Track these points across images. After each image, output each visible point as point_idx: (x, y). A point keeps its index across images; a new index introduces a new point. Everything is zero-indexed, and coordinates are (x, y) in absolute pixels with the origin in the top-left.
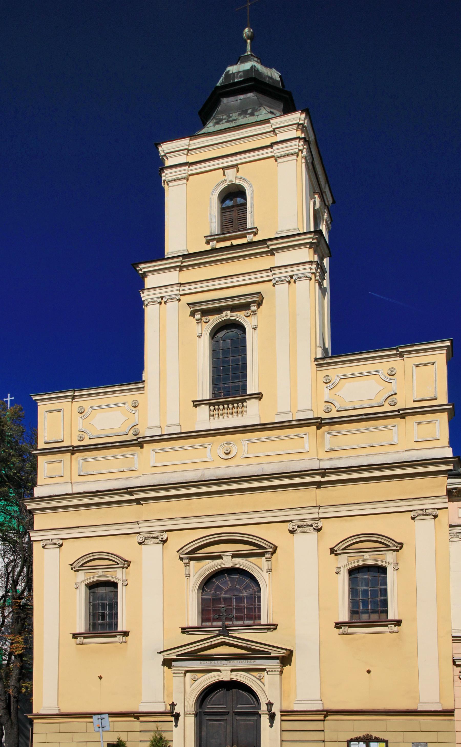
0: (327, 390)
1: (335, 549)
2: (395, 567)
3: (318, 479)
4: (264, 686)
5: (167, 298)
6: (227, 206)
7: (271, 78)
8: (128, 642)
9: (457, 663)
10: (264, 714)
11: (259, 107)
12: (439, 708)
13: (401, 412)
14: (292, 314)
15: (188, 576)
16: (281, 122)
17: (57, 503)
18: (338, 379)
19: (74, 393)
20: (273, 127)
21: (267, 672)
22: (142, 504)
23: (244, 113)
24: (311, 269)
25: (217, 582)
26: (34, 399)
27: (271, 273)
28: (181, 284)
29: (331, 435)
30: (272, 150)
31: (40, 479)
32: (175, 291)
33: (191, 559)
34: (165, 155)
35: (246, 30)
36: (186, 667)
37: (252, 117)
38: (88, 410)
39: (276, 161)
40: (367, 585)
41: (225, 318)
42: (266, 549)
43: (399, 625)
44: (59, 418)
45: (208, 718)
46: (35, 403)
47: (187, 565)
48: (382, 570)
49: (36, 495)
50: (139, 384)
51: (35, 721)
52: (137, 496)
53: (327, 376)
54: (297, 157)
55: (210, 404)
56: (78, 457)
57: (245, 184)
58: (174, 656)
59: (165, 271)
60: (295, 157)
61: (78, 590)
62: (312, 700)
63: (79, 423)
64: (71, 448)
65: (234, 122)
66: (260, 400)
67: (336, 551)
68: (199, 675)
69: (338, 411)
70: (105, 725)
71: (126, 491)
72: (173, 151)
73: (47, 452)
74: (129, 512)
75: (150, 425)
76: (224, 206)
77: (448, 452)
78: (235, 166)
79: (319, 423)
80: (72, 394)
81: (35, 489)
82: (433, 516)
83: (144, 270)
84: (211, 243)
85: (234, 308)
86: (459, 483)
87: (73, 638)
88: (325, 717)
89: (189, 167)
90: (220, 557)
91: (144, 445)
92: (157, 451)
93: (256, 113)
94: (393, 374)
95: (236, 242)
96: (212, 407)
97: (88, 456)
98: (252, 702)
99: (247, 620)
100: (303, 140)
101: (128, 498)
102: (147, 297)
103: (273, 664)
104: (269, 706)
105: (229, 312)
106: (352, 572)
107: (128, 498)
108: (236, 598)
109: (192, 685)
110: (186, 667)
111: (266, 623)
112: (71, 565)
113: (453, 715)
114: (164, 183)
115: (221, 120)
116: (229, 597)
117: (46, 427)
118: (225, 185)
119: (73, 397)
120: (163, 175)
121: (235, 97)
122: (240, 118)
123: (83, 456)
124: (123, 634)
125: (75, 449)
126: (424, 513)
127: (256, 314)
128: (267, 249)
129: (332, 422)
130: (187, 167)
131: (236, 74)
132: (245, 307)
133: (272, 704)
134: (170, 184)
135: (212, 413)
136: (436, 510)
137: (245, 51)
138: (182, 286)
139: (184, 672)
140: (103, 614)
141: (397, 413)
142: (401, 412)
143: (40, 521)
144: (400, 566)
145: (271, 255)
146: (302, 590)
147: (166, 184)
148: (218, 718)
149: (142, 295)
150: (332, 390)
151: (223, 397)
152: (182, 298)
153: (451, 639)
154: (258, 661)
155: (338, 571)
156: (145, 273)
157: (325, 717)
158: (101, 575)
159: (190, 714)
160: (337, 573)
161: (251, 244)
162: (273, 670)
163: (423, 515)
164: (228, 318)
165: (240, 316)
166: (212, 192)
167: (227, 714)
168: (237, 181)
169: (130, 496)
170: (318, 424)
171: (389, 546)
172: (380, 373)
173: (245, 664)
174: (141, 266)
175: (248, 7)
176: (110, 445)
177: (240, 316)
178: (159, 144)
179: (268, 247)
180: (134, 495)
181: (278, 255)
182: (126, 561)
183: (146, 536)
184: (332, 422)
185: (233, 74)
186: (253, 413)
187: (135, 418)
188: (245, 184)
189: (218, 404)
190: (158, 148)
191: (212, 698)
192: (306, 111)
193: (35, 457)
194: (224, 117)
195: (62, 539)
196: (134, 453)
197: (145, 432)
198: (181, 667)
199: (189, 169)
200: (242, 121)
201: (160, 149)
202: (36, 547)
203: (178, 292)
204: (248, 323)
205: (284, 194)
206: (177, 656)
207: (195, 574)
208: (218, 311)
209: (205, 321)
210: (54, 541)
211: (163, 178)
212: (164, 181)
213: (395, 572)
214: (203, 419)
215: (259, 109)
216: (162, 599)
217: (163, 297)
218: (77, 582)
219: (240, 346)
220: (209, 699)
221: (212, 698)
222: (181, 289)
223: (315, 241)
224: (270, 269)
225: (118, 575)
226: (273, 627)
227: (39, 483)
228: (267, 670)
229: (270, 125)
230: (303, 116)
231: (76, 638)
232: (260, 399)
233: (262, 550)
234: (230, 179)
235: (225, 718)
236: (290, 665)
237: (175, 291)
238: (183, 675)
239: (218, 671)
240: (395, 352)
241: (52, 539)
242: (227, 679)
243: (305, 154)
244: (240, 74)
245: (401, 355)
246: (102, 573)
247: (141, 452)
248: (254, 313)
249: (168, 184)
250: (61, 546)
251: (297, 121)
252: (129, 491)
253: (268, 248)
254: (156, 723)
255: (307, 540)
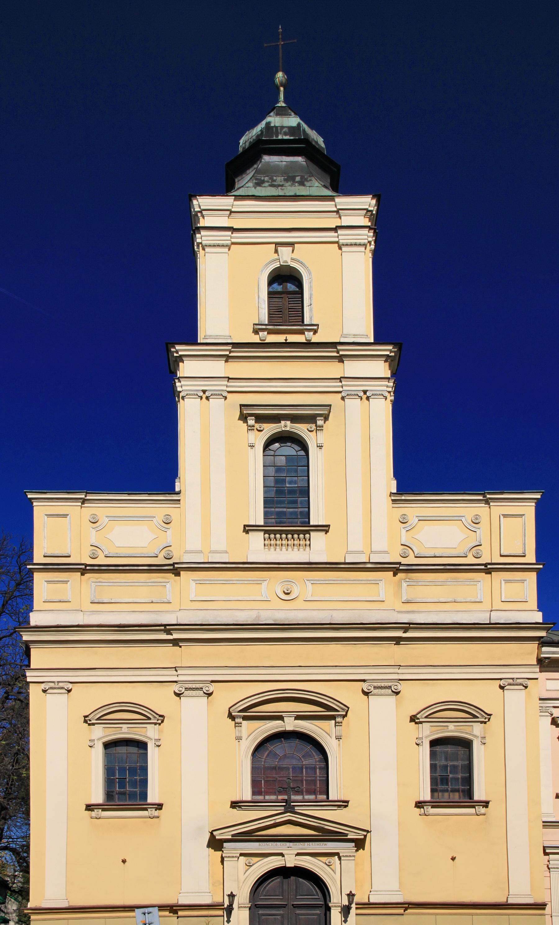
0: (404, 531)
1: (418, 716)
2: (158, 743)
3: (399, 634)
4: (335, 873)
5: (211, 393)
6: (274, 290)
7: (317, 142)
8: (161, 817)
9: (547, 851)
10: (335, 906)
11: (310, 176)
12: (531, 901)
13: (489, 566)
14: (357, 443)
15: (239, 739)
16: (347, 203)
17: (65, 635)
18: (417, 520)
19: (86, 496)
20: (338, 207)
21: (340, 859)
22: (180, 647)
23: (291, 179)
24: (387, 386)
25: (270, 747)
26: (29, 496)
27: (340, 384)
28: (229, 378)
29: (408, 583)
30: (336, 234)
31: (37, 603)
32: (222, 386)
33: (245, 718)
34: (201, 212)
35: (280, 75)
36: (241, 849)
37: (302, 188)
38: (103, 520)
39: (340, 248)
40: (446, 759)
41: (283, 429)
42: (337, 711)
43: (487, 807)
44: (62, 525)
45: (260, 912)
46: (30, 502)
47: (238, 725)
48: (467, 744)
49: (33, 623)
50: (173, 495)
51: (33, 917)
52: (176, 636)
53: (404, 515)
54: (365, 249)
55: (266, 532)
56: (90, 578)
57: (285, 266)
58: (229, 835)
59: (197, 359)
60: (363, 249)
61: (421, 747)
62: (385, 891)
63: (93, 537)
64: (83, 567)
65: (280, 188)
66: (326, 533)
67: (418, 719)
68: (255, 859)
69: (416, 557)
70: (153, 921)
71: (163, 628)
72: (211, 209)
73: (47, 568)
74: (164, 655)
75: (188, 548)
76: (271, 290)
77: (538, 617)
78: (292, 244)
79: (396, 569)
80: (83, 496)
81: (31, 614)
82: (524, 686)
83: (180, 353)
84: (261, 333)
85: (295, 419)
86: (554, 653)
87: (86, 809)
88: (404, 911)
89: (232, 233)
90: (281, 718)
91: (181, 572)
92: (198, 582)
93: (307, 184)
94: (477, 521)
95: (292, 338)
96: (267, 535)
97: (104, 579)
98: (315, 892)
99: (306, 795)
100: (372, 231)
101: (164, 636)
102: (184, 388)
103: (348, 848)
104: (351, 897)
105: (288, 423)
106: (434, 743)
107: (164, 636)
108: (292, 768)
109: (246, 871)
110: (241, 849)
111: (336, 799)
112: (85, 717)
113: (544, 909)
114: (198, 246)
115: (263, 182)
116: (291, 766)
117: (46, 536)
118: (277, 265)
119: (84, 501)
120: (198, 236)
121: (280, 157)
122: (287, 184)
123: (97, 579)
124: (156, 806)
125: (88, 568)
126: (514, 682)
127: (322, 430)
128: (335, 354)
129: (411, 569)
130: (230, 233)
131: (279, 128)
132: (311, 419)
133: (354, 895)
134: (207, 250)
135: (266, 542)
136: (527, 680)
137: (277, 101)
138: (230, 381)
139: (238, 855)
140: (126, 779)
141: (483, 567)
142: (489, 566)
143: (38, 657)
144: (487, 741)
145: (339, 362)
146: (376, 764)
147: (201, 248)
148: (273, 912)
149: (178, 384)
150: (409, 532)
151: (299, 525)
152: (229, 396)
153: (542, 824)
154: (330, 844)
155: (91, 744)
156: (181, 356)
157: (404, 911)
158: (125, 732)
159: (245, 907)
160: (418, 745)
161: (309, 344)
162: (348, 854)
163: (513, 685)
164: (288, 429)
165: (301, 429)
166: (262, 271)
167: (285, 907)
168: (292, 263)
169: (167, 634)
170: (395, 570)
171: (478, 717)
172: (463, 519)
173: (314, 846)
174: (178, 347)
175: (280, 46)
176: (136, 568)
177: (301, 429)
178: (195, 196)
179: (335, 350)
180: (172, 635)
181: (348, 363)
182: (160, 716)
183: (187, 686)
184: (411, 569)
185: (276, 127)
186: (319, 548)
187: (169, 537)
188: (285, 266)
189: (275, 532)
190: (191, 200)
191: (265, 888)
192: (377, 197)
193: (31, 573)
194: (266, 179)
195: (71, 683)
196: (167, 581)
197: (180, 556)
198: (235, 849)
199: (232, 235)
200: (291, 190)
201: (195, 202)
202: (34, 692)
203: (224, 388)
204: (311, 440)
205: (344, 290)
206: (233, 836)
207: (249, 736)
208: (276, 419)
209: (259, 429)
210: (61, 685)
211: (199, 240)
212: (198, 244)
213: (483, 746)
214: (257, 548)
215: (309, 179)
216: (203, 765)
217: (206, 390)
218: (92, 739)
219: (301, 464)
220: (262, 888)
221: (265, 888)
222: (229, 384)
223: (393, 354)
224: (340, 379)
225: (149, 733)
226: (345, 804)
227: (35, 608)
228: (341, 855)
229: (333, 203)
230: (374, 202)
231: (92, 810)
232: (327, 532)
233: (331, 712)
234: (285, 259)
235: (281, 912)
236: (364, 849)
237: (222, 386)
238: (237, 859)
239: (282, 855)
240: (481, 498)
241: (58, 682)
242: (290, 864)
243: (373, 247)
244: (284, 130)
245: (487, 502)
246: (127, 729)
247: (175, 581)
248: (319, 428)
249: (204, 249)
250: (69, 691)
251: (367, 207)
252: (167, 628)
253: (338, 352)
254: (206, 918)
255: (382, 704)
